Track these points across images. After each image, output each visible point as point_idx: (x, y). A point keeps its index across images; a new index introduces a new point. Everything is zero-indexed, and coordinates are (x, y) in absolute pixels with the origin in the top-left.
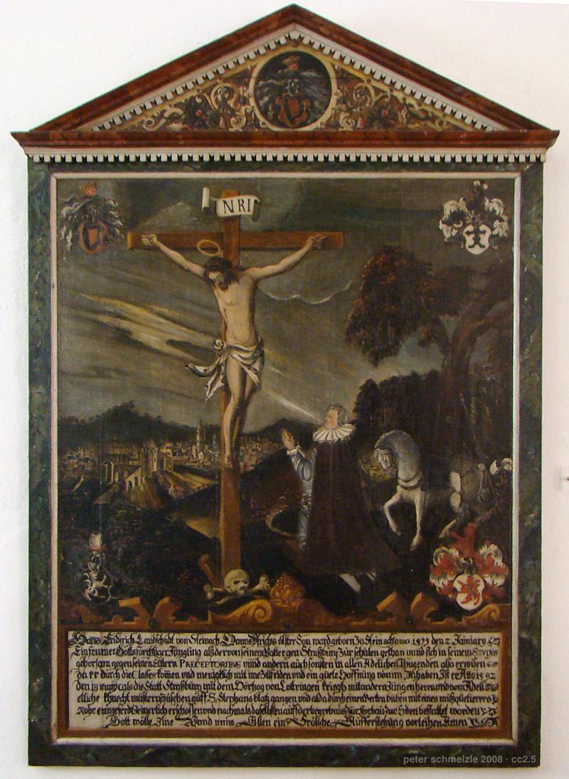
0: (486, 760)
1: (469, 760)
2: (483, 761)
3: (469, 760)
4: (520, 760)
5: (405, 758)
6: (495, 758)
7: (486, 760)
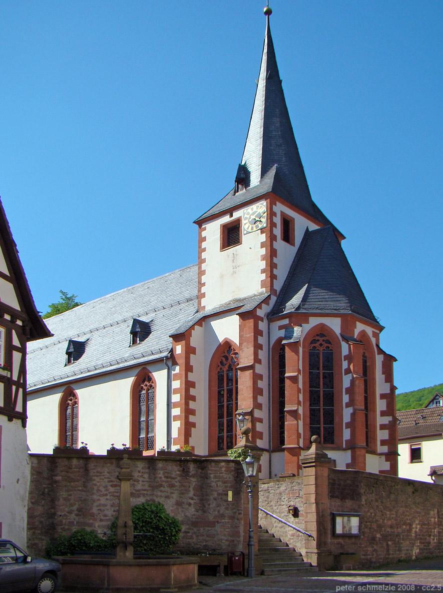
0: (401, 588)
1: (388, 588)
2: (399, 589)
3: (388, 588)
4: (364, 588)
5: (337, 587)
6: (404, 589)
7: (401, 588)
